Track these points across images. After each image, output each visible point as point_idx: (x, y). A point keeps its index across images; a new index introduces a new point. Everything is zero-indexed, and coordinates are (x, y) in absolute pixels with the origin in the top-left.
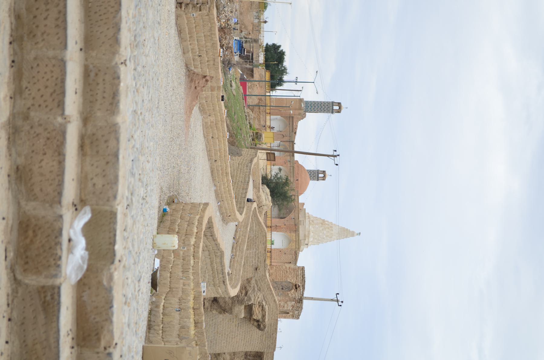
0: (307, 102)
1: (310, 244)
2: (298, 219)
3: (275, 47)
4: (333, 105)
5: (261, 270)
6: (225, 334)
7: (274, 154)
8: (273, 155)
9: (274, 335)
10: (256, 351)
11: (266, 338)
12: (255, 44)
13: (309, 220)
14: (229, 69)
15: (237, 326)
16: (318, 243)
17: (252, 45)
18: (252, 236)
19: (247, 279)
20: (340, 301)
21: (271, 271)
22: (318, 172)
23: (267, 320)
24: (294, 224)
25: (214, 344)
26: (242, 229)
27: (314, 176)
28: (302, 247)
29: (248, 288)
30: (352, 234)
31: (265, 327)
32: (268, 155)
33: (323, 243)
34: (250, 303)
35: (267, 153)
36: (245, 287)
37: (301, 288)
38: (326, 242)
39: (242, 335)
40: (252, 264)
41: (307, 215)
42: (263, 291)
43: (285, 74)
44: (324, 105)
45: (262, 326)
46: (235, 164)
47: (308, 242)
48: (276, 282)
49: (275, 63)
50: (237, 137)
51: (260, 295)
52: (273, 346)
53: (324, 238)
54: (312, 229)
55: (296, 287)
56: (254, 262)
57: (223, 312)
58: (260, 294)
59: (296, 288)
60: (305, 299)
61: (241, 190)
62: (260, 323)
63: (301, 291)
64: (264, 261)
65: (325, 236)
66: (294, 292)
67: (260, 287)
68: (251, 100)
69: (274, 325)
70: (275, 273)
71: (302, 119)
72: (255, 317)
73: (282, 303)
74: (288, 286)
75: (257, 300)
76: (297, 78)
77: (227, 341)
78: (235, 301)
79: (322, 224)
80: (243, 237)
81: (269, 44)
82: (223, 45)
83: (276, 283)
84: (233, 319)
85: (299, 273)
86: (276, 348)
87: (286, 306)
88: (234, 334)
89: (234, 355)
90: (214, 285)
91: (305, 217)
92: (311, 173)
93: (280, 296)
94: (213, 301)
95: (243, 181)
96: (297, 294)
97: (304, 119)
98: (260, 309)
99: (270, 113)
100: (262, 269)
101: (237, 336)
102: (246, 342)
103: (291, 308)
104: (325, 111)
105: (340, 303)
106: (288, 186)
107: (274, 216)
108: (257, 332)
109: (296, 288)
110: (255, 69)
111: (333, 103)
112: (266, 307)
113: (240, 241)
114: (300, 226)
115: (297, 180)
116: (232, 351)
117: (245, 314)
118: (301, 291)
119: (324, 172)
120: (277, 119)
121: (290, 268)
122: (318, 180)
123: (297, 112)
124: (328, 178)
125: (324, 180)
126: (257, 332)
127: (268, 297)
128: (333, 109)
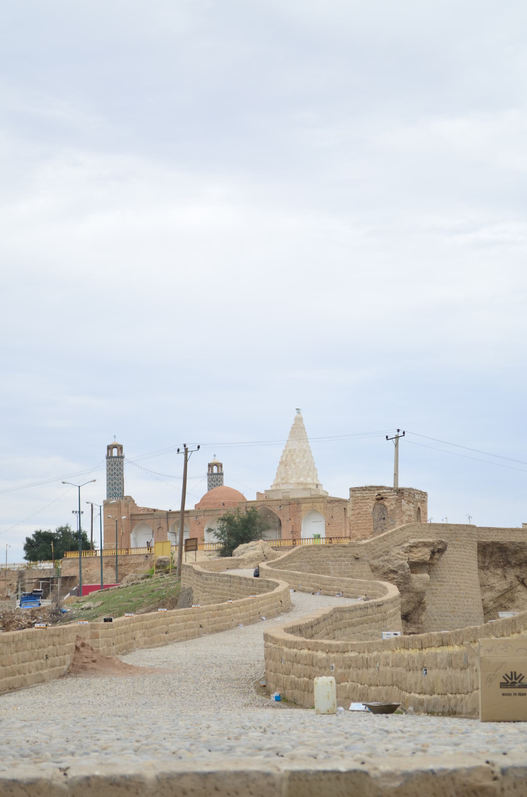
0: (109, 495)
1: (316, 482)
2: (280, 500)
4: (112, 457)
5: (357, 552)
6: (455, 601)
7: (187, 540)
8: (189, 542)
9: (452, 528)
10: (476, 553)
11: (456, 540)
12: (26, 577)
13: (281, 485)
14: (64, 613)
15: (442, 583)
16: (315, 469)
17: (27, 581)
18: (308, 567)
19: (373, 571)
21: (359, 537)
22: (210, 474)
23: (431, 540)
25: (470, 617)
26: (300, 582)
27: (217, 480)
28: (321, 493)
29: (385, 570)
30: (299, 420)
31: (442, 542)
32: (189, 548)
34: (408, 566)
35: (186, 550)
36: (385, 573)
37: (382, 491)
38: (312, 458)
39: (455, 575)
40: (350, 566)
41: (274, 488)
42: (388, 547)
43: (68, 530)
45: (440, 547)
46: (205, 597)
47: (313, 484)
48: (374, 528)
49: (52, 545)
50: (164, 597)
53: (307, 462)
54: (294, 479)
56: (347, 563)
57: (423, 605)
58: (393, 551)
59: (382, 498)
61: (242, 587)
62: (436, 550)
63: (385, 491)
64: (344, 548)
65: (304, 461)
66: (388, 502)
67: (383, 552)
68: (109, 578)
69: (437, 529)
70: (362, 530)
71: (134, 501)
74: (380, 511)
75: (402, 555)
76: (73, 512)
77: (465, 597)
78: (406, 588)
79: (286, 465)
80: (312, 580)
81: (25, 555)
82: (29, 623)
83: (375, 529)
84: (432, 589)
85: (359, 495)
87: (408, 513)
88: (453, 588)
89: (485, 586)
90: (384, 620)
91: (277, 490)
93: (395, 522)
94: (408, 621)
95: (229, 584)
98: (415, 550)
99: (127, 549)
100: (356, 551)
101: (457, 583)
102: (464, 568)
103: (411, 504)
104: (120, 469)
105: (401, 434)
106: (234, 517)
107: (278, 536)
108: (449, 554)
109: (382, 498)
110: (63, 575)
111: (108, 457)
112: (412, 541)
113: (317, 584)
114: (291, 497)
115: (224, 504)
116: (478, 589)
118: (385, 491)
119: (210, 466)
120: (135, 539)
121: (352, 510)
122: (222, 474)
124: (218, 460)
125: (221, 466)
126: (449, 554)
127: (397, 540)
128: (118, 457)
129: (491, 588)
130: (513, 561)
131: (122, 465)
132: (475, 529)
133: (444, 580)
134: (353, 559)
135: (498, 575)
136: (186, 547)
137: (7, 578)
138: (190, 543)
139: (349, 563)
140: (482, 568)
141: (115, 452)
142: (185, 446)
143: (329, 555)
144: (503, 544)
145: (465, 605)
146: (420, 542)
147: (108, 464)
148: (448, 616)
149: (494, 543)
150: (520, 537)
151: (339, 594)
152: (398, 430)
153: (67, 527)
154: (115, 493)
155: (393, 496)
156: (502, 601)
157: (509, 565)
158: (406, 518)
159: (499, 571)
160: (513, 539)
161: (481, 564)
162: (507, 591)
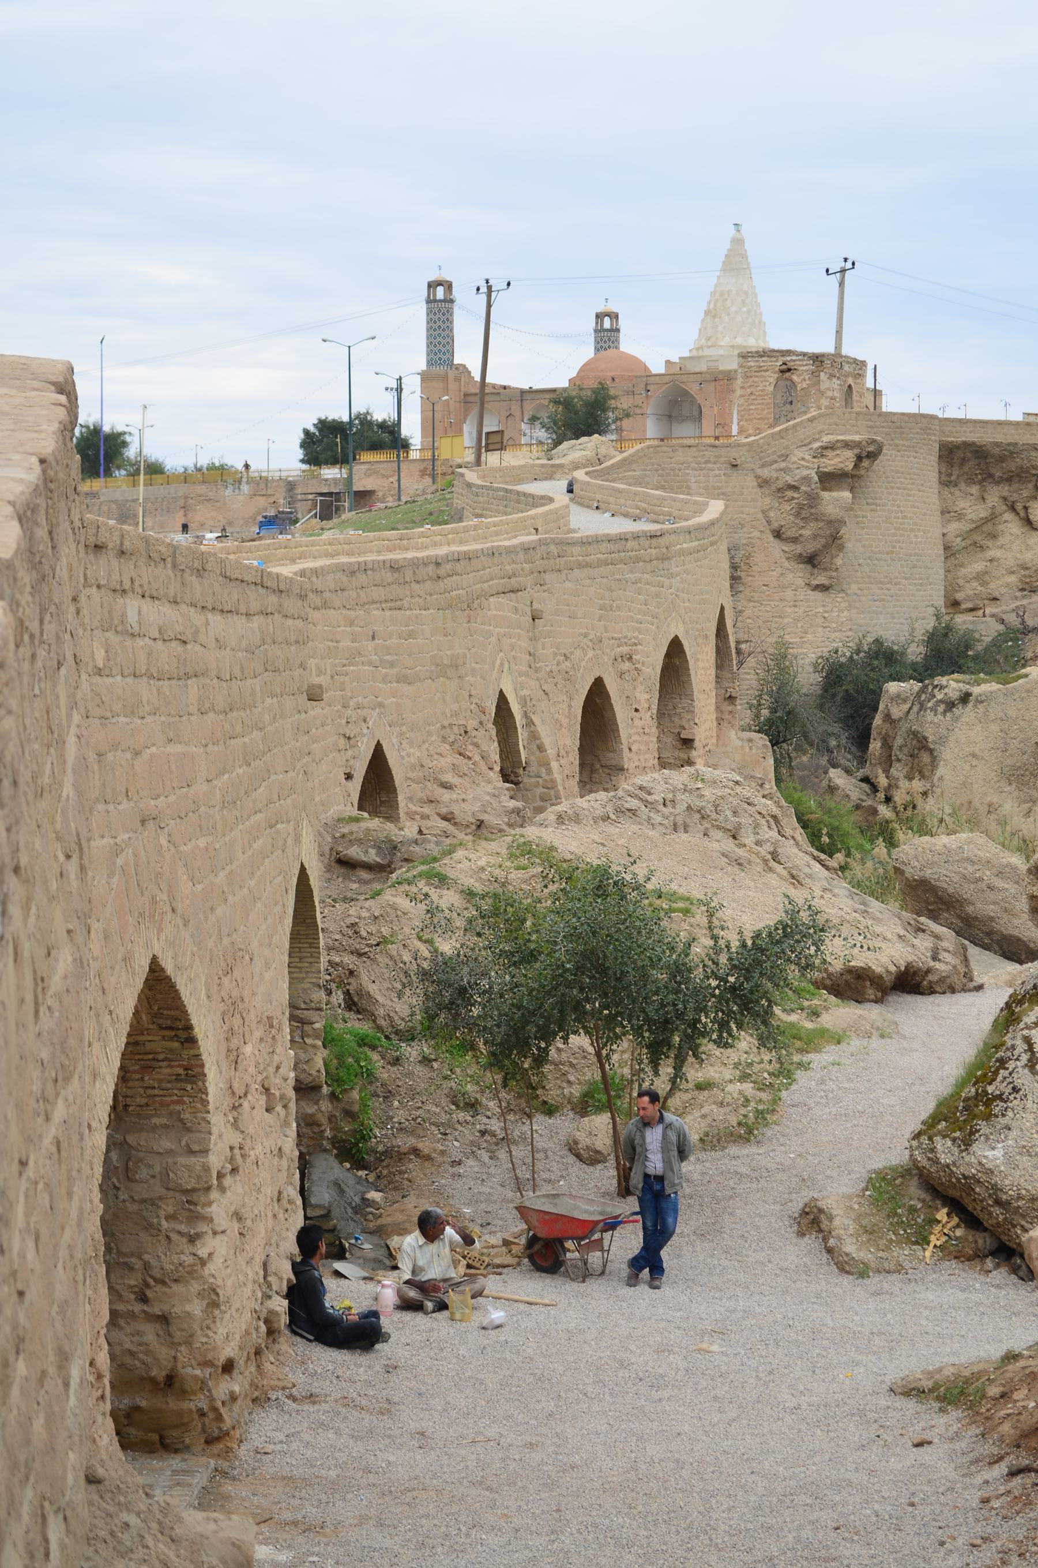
0: (430, 363)
2: (701, 373)
3: (309, 442)
4: (435, 301)
5: (736, 455)
6: (894, 535)
7: (488, 434)
8: (491, 436)
9: (895, 419)
10: (936, 460)
11: (902, 439)
12: (299, 490)
13: (705, 349)
15: (874, 507)
17: (299, 497)
18: (656, 478)
19: (760, 486)
20: (843, 264)
21: (750, 432)
22: (599, 330)
23: (857, 438)
24: (713, 383)
25: (918, 561)
26: (623, 501)
27: (609, 340)
29: (780, 484)
30: (738, 242)
31: (874, 441)
32: (491, 447)
33: (761, 313)
34: (816, 478)
35: (487, 451)
36: (779, 490)
37: (789, 358)
38: (758, 305)
39: (897, 494)
41: (695, 353)
42: (787, 447)
43: (369, 418)
44: (435, 322)
45: (871, 449)
49: (338, 440)
51: (799, 454)
52: (923, 420)
53: (749, 311)
54: (727, 339)
55: (786, 370)
56: (717, 472)
57: (839, 542)
58: (795, 456)
59: (789, 370)
60: (840, 348)
62: (864, 454)
63: (794, 358)
64: (714, 449)
65: (744, 309)
66: (798, 376)
67: (779, 457)
69: (870, 420)
71: (470, 373)
72: (850, 466)
73: (825, 402)
74: (785, 390)
75: (808, 462)
76: (387, 389)
77: (912, 530)
78: (811, 514)
79: (714, 317)
80: (637, 498)
81: (302, 457)
84: (856, 516)
85: (752, 364)
86: (1008, 419)
87: (830, 394)
88: (893, 514)
89: (949, 512)
90: (666, 558)
91: (699, 357)
92: (601, 347)
93: (808, 408)
94: (814, 566)
96: (804, 368)
97: (470, 369)
98: (830, 454)
100: (734, 453)
101: (899, 507)
102: (913, 484)
103: (834, 380)
104: (448, 320)
105: (849, 265)
106: (573, 399)
107: (697, 431)
108: (888, 460)
109: (789, 370)
110: (355, 488)
111: (429, 301)
112: (826, 439)
113: (644, 505)
114: (721, 368)
116: (937, 517)
117: (843, 490)
118: (794, 358)
119: (599, 317)
121: (742, 388)
122: (618, 330)
123: (453, 386)
124: (612, 307)
125: (617, 316)
126: (888, 460)
127: (802, 437)
128: (444, 301)
129: (960, 516)
130: (998, 474)
131: (452, 315)
132: (936, 422)
133: (878, 501)
134: (729, 466)
135: (972, 495)
136: (487, 445)
137: (269, 492)
138: (493, 439)
139: (722, 473)
140: (946, 483)
141: (440, 293)
142: (487, 282)
143: (690, 460)
144: (981, 446)
145: (911, 543)
146: (838, 441)
147: (429, 312)
148: (881, 560)
149: (966, 445)
150: (1012, 435)
151: (669, 520)
152: (846, 260)
153: (368, 413)
154: (440, 359)
155: (807, 367)
156: (977, 537)
157: (990, 480)
158: (825, 402)
159: (975, 490)
160: (1000, 438)
161: (944, 478)
162: (986, 521)
